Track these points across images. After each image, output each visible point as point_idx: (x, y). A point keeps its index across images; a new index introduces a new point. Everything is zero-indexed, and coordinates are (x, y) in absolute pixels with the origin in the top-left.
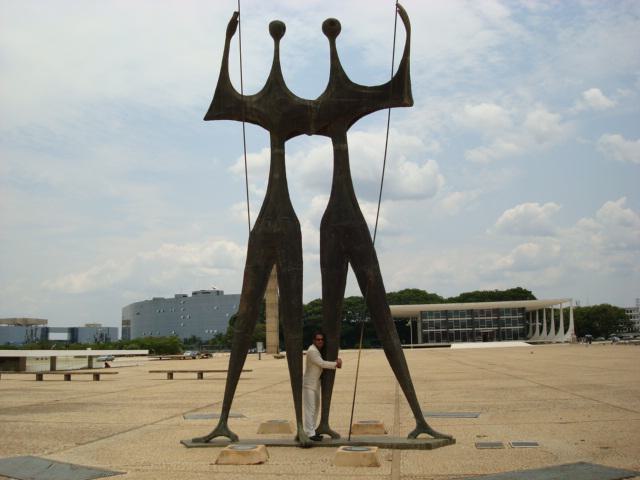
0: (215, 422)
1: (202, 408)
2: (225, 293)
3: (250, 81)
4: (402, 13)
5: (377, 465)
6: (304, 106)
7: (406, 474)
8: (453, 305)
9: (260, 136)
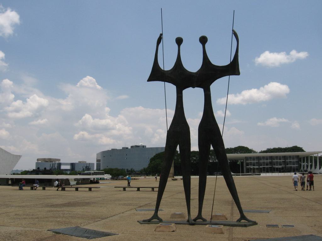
0: (153, 212)
1: (142, 206)
2: (147, 147)
3: (167, 65)
4: (235, 34)
5: (222, 233)
6: (191, 74)
7: (235, 237)
8: (262, 154)
9: (171, 89)
